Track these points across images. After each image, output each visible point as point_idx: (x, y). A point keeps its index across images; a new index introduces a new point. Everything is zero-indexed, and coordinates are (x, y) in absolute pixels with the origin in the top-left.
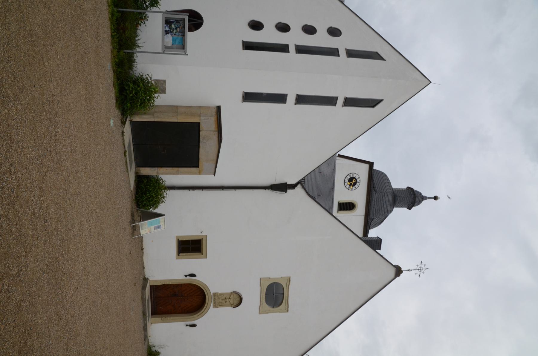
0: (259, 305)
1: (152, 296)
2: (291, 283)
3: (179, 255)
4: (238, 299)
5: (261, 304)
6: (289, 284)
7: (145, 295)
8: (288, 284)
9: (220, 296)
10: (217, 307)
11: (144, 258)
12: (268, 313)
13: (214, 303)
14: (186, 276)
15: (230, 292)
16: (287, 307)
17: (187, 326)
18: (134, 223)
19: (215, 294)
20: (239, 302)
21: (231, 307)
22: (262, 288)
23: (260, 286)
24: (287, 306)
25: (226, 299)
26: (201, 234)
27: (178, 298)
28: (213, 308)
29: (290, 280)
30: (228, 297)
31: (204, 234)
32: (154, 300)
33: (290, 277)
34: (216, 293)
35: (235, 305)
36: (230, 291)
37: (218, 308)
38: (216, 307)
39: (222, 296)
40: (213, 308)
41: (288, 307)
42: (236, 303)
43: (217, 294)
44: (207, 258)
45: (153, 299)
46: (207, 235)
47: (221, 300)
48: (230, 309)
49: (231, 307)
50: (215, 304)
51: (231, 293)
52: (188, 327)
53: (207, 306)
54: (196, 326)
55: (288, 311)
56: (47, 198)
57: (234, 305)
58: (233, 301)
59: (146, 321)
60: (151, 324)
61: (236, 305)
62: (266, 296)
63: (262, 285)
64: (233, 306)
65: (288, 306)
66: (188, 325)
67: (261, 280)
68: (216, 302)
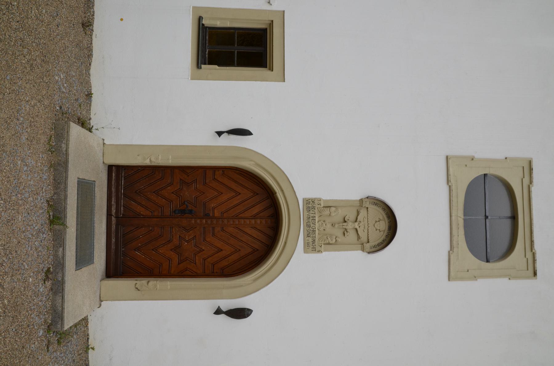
0: (448, 248)
1: (114, 211)
2: (535, 181)
3: (198, 67)
4: (383, 225)
5: (455, 243)
6: (531, 182)
7: (68, 140)
8: (526, 181)
9: (327, 212)
10: (318, 248)
11: (92, 71)
12: (475, 278)
13: (308, 236)
14: (220, 133)
15: (359, 198)
16: (531, 261)
17: (218, 312)
18: (123, 206)
19: (310, 203)
20: (386, 233)
21: (363, 250)
22: (454, 188)
23: (448, 181)
24: (529, 255)
25: (345, 222)
26: (267, 7)
27: (193, 221)
28: (306, 251)
29: (531, 169)
30: (351, 216)
31: (276, 6)
32: (117, 225)
33: (532, 159)
34: (312, 201)
35: (374, 247)
36: (355, 195)
37: (319, 251)
38: (314, 250)
39: (333, 209)
40: (306, 251)
41: (534, 261)
42: (377, 237)
43: (316, 202)
44: (284, 81)
45: (113, 219)
46: (284, 11)
47: (329, 226)
48: (358, 255)
49: (360, 253)
50: (310, 240)
51: (361, 200)
52: (223, 317)
53: (285, 243)
54: (248, 315)
55: (535, 274)
56: (41, 260)
57: (372, 243)
58: (366, 231)
59: (61, 249)
60: (101, 301)
61: (376, 243)
62: (465, 220)
63: (452, 178)
64: (367, 246)
65: (534, 255)
66: (224, 310)
67: (450, 161)
68: (314, 231)
